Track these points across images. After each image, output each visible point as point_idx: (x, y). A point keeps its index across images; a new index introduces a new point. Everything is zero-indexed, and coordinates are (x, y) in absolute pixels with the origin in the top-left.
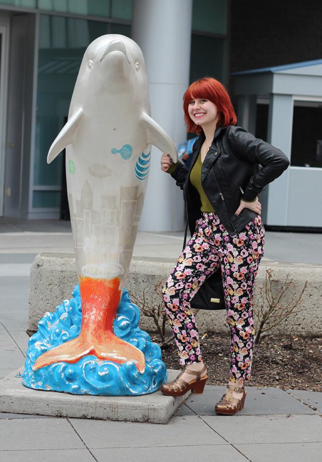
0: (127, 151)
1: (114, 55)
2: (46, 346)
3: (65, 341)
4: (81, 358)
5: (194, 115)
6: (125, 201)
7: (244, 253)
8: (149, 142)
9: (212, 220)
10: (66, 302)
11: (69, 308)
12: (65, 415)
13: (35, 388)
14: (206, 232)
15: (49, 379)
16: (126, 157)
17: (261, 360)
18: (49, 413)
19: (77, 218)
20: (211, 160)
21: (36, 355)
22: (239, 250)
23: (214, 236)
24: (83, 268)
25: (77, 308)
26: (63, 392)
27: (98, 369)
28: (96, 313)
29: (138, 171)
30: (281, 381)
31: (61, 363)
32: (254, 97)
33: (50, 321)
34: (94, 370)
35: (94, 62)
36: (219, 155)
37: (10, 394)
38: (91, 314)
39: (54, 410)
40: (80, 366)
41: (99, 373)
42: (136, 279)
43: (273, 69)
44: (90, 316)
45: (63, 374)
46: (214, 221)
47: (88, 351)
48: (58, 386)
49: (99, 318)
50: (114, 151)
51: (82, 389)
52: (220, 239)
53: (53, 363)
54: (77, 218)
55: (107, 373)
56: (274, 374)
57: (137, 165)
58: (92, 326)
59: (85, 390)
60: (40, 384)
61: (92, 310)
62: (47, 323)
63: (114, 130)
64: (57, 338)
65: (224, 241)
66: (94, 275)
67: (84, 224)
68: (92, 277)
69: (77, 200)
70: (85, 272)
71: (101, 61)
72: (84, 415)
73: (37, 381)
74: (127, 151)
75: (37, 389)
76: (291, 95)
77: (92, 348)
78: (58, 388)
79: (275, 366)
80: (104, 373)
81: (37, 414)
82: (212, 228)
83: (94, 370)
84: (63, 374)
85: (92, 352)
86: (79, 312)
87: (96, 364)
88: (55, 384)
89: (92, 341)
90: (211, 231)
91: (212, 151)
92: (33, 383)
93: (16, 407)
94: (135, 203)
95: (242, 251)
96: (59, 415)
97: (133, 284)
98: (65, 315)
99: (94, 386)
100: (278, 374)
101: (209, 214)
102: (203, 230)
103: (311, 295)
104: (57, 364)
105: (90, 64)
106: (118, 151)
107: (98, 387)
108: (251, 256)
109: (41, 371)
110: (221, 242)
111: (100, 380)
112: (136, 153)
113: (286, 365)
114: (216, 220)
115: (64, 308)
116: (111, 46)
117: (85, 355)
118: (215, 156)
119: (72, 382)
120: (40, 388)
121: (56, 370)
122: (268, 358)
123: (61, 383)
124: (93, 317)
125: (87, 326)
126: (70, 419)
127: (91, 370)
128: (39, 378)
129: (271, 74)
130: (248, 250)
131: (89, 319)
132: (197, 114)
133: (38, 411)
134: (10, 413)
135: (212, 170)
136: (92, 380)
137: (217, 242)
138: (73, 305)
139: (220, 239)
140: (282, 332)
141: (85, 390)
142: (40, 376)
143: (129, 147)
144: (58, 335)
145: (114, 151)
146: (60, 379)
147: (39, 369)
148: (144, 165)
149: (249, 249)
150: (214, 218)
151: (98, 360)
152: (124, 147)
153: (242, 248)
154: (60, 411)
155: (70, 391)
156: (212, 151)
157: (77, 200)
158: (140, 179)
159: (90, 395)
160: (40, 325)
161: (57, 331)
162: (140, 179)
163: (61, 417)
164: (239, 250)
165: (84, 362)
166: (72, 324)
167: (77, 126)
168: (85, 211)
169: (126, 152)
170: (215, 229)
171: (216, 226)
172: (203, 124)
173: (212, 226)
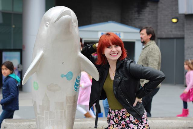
0: (70, 76)
2: (85, 93)
6: (69, 104)
7: (140, 127)
8: (81, 69)
9: (117, 114)
14: (115, 121)
16: (69, 79)
19: (40, 116)
20: (118, 82)
22: (137, 125)
23: (120, 122)
29: (76, 86)
35: (49, 23)
36: (122, 79)
46: (119, 114)
50: (62, 76)
52: (125, 123)
57: (75, 83)
65: (127, 124)
67: (45, 119)
69: (39, 105)
74: (70, 76)
82: (118, 119)
90: (118, 120)
91: (117, 77)
94: (74, 105)
95: (139, 126)
101: (115, 111)
102: (113, 120)
105: (47, 24)
106: (65, 76)
108: (145, 127)
110: (126, 125)
112: (75, 77)
114: (120, 114)
116: (63, 13)
118: (120, 79)
130: (142, 125)
135: (119, 88)
137: (123, 125)
139: (125, 123)
143: (71, 73)
145: (62, 76)
148: (77, 86)
149: (142, 124)
150: (119, 113)
152: (68, 73)
153: (138, 124)
156: (117, 77)
157: (39, 105)
158: (76, 91)
162: (76, 91)
164: (137, 125)
167: (39, 62)
168: (45, 111)
169: (69, 76)
170: (120, 118)
171: (121, 117)
173: (118, 117)
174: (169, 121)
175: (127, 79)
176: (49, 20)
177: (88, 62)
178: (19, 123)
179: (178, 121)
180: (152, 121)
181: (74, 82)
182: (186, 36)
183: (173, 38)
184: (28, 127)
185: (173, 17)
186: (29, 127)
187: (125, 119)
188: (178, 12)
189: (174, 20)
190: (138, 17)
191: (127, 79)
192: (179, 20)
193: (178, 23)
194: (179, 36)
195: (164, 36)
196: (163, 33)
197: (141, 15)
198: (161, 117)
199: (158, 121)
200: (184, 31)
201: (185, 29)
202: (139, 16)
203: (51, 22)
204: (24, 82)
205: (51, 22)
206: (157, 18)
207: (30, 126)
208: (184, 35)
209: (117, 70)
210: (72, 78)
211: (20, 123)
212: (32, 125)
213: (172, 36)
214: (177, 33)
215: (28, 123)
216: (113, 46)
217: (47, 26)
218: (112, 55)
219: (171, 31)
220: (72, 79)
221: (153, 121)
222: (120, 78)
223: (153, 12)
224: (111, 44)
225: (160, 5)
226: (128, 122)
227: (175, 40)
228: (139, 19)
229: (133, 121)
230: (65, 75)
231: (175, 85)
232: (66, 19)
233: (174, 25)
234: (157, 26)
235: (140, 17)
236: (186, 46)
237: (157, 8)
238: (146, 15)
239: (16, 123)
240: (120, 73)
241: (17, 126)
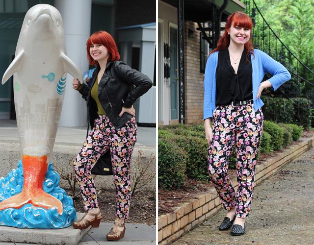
3: (13, 195)
4: (23, 205)
6: (50, 108)
9: (105, 120)
33: (4, 182)
36: (109, 79)
39: (6, 238)
41: (34, 215)
47: (27, 201)
49: (34, 181)
50: (44, 77)
52: (110, 131)
53: (5, 208)
57: (58, 85)
58: (30, 186)
65: (112, 133)
82: (105, 125)
83: (31, 213)
85: (30, 202)
87: (32, 209)
89: (30, 195)
100: (146, 215)
106: (46, 77)
110: (110, 133)
112: (57, 79)
123: (10, 221)
124: (30, 180)
125: (27, 185)
136: (30, 219)
137: (107, 133)
138: (18, 172)
139: (110, 131)
145: (44, 77)
146: (10, 218)
151: (33, 206)
161: (8, 188)
163: (10, 242)
165: (25, 208)
166: (17, 185)
168: (25, 114)
169: (50, 78)
171: (107, 123)
175: (114, 80)
177: (70, 63)
181: (56, 84)
187: (111, 127)
191: (114, 80)
204: (12, 69)
209: (106, 71)
210: (53, 80)
216: (95, 45)
217: (29, 25)
220: (54, 81)
222: (107, 78)
224: (92, 43)
226: (246, 143)
229: (221, 140)
230: (47, 75)
232: (44, 18)
240: (108, 73)
241: (12, 147)
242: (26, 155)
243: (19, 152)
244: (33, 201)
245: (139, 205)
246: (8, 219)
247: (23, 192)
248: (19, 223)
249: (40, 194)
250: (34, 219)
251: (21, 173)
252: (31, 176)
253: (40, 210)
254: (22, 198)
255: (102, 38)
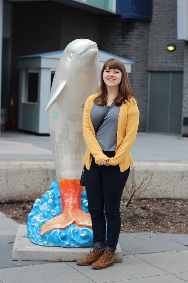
1: (93, 51)
3: (54, 216)
4: (68, 226)
5: (108, 79)
10: (49, 193)
11: (52, 196)
12: (63, 261)
13: (42, 245)
15: (52, 239)
17: (134, 216)
18: (54, 259)
19: (58, 145)
21: (39, 225)
24: (62, 174)
25: (56, 196)
26: (60, 247)
27: (80, 232)
28: (72, 199)
30: (146, 229)
31: (58, 230)
32: (27, 69)
33: (40, 204)
34: (77, 233)
37: (30, 250)
38: (70, 199)
39: (57, 258)
40: (69, 231)
41: (81, 235)
42: (47, 172)
43: (42, 55)
44: (69, 201)
45: (59, 236)
47: (72, 222)
48: (57, 243)
49: (75, 202)
51: (71, 244)
53: (52, 230)
54: (58, 145)
55: (86, 234)
56: (144, 224)
58: (71, 207)
59: (73, 245)
60: (45, 242)
61: (69, 198)
62: (38, 205)
63: (84, 94)
64: (49, 215)
66: (69, 177)
68: (68, 178)
70: (64, 176)
71: (81, 54)
72: (75, 260)
73: (43, 240)
75: (44, 245)
76: (49, 69)
77: (74, 220)
78: (57, 244)
79: (142, 219)
80: (84, 235)
81: (47, 261)
83: (77, 233)
84: (59, 236)
85: (74, 222)
86: (58, 198)
87: (78, 229)
88: (55, 242)
89: (73, 216)
92: (41, 242)
93: (34, 257)
96: (60, 260)
97: (45, 175)
98: (50, 201)
99: (79, 242)
100: (146, 224)
103: (139, 178)
104: (55, 231)
107: (81, 243)
109: (46, 235)
111: (82, 239)
113: (147, 218)
115: (49, 196)
116: (90, 46)
117: (71, 224)
119: (65, 241)
120: (45, 245)
121: (55, 233)
122: (138, 215)
123: (59, 241)
124: (71, 202)
125: (68, 207)
126: (67, 263)
127: (76, 233)
128: (45, 239)
129: (40, 58)
131: (68, 203)
132: (111, 79)
133: (47, 259)
134: (30, 261)
136: (76, 239)
138: (53, 194)
140: (124, 198)
141: (73, 245)
142: (45, 238)
144: (49, 212)
146: (58, 239)
147: (45, 234)
151: (78, 226)
154: (60, 258)
155: (65, 246)
159: (76, 247)
160: (35, 207)
161: (48, 210)
163: (61, 261)
165: (71, 229)
166: (55, 206)
168: (64, 140)
172: (108, 86)
174: (173, 164)
176: (73, 52)
178: (8, 162)
179: (183, 164)
180: (155, 164)
182: (185, 70)
183: (169, 72)
184: (19, 167)
185: (170, 43)
186: (20, 167)
188: (176, 38)
189: (171, 48)
190: (122, 43)
192: (177, 48)
193: (175, 52)
194: (177, 70)
195: (157, 70)
196: (155, 64)
197: (126, 39)
198: (165, 161)
199: (162, 164)
200: (182, 63)
201: (185, 60)
202: (124, 41)
203: (75, 54)
205: (75, 54)
206: (147, 44)
207: (21, 166)
208: (183, 68)
211: (10, 163)
212: (23, 164)
213: (167, 70)
214: (174, 65)
215: (19, 163)
217: (71, 58)
218: (109, 80)
219: (166, 63)
221: (156, 164)
223: (142, 36)
225: (152, 27)
227: (171, 74)
228: (123, 44)
231: (169, 134)
233: (170, 55)
234: (148, 54)
235: (125, 43)
236: (185, 82)
237: (149, 30)
238: (133, 39)
239: (6, 162)
242: (65, 179)
243: (14, 170)
244: (77, 222)
245: (137, 215)
246: (88, 250)
247: (64, 214)
248: (67, 243)
249: (81, 214)
250: (81, 238)
251: (57, 194)
252: (71, 198)
253: (87, 230)
254: (65, 219)
255: (116, 65)
